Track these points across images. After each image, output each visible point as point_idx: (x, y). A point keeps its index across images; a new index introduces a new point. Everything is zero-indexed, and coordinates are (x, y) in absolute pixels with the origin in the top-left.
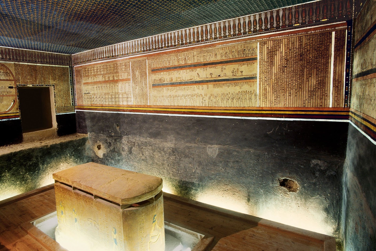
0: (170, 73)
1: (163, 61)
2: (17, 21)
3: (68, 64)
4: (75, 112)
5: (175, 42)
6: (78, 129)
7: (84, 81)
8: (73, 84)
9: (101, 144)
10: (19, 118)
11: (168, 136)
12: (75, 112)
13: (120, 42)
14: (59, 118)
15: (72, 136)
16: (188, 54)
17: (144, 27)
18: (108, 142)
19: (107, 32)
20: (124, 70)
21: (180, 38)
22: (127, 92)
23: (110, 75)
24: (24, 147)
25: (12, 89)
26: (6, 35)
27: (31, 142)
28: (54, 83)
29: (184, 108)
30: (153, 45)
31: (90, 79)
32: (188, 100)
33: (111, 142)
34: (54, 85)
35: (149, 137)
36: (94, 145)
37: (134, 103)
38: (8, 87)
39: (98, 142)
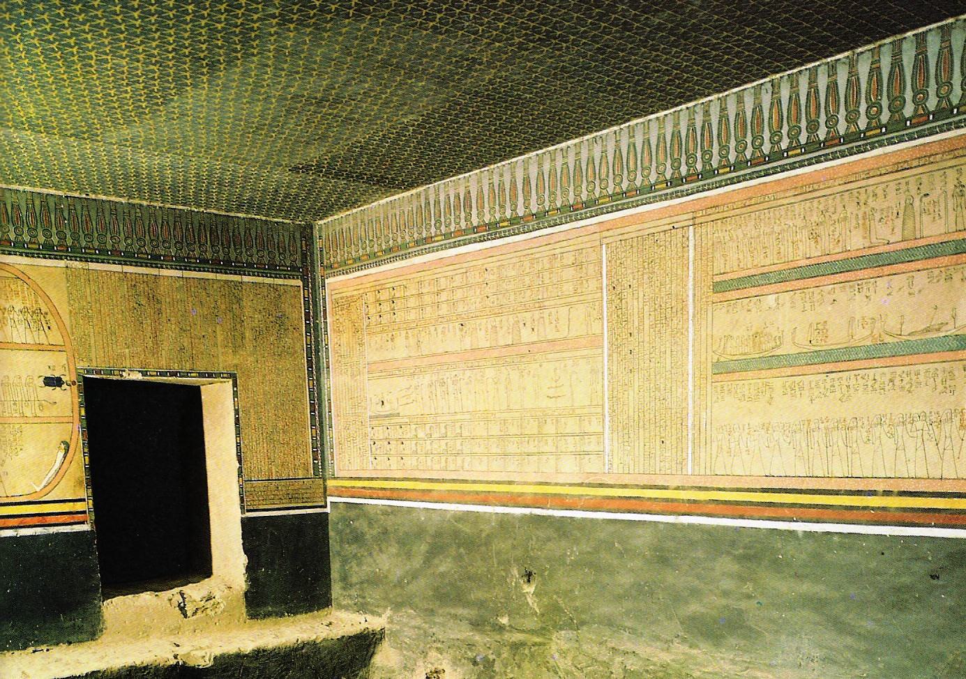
0: (816, 297)
1: (777, 229)
2: (72, 41)
3: (294, 268)
4: (325, 507)
5: (852, 119)
6: (336, 590)
7: (372, 355)
8: (315, 365)
9: (445, 665)
10: (86, 527)
11: (784, 637)
12: (325, 507)
13: (553, 141)
14: (252, 530)
15: (310, 621)
16: (925, 179)
17: (685, 36)
18: (478, 659)
19: (490, 82)
20: (568, 288)
21: (885, 93)
22: (583, 407)
23: (498, 319)
24: (106, 659)
25: (58, 388)
26: (29, 120)
27: (136, 637)
28: (235, 362)
29: (880, 488)
30: (728, 141)
31: (400, 340)
32: (910, 444)
33: (491, 657)
34: (233, 376)
35: (684, 640)
36: (413, 670)
37: (616, 461)
38: (41, 382)
39: (433, 654)
